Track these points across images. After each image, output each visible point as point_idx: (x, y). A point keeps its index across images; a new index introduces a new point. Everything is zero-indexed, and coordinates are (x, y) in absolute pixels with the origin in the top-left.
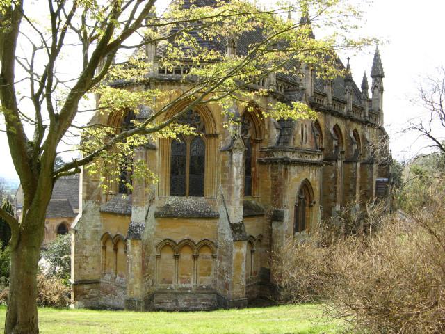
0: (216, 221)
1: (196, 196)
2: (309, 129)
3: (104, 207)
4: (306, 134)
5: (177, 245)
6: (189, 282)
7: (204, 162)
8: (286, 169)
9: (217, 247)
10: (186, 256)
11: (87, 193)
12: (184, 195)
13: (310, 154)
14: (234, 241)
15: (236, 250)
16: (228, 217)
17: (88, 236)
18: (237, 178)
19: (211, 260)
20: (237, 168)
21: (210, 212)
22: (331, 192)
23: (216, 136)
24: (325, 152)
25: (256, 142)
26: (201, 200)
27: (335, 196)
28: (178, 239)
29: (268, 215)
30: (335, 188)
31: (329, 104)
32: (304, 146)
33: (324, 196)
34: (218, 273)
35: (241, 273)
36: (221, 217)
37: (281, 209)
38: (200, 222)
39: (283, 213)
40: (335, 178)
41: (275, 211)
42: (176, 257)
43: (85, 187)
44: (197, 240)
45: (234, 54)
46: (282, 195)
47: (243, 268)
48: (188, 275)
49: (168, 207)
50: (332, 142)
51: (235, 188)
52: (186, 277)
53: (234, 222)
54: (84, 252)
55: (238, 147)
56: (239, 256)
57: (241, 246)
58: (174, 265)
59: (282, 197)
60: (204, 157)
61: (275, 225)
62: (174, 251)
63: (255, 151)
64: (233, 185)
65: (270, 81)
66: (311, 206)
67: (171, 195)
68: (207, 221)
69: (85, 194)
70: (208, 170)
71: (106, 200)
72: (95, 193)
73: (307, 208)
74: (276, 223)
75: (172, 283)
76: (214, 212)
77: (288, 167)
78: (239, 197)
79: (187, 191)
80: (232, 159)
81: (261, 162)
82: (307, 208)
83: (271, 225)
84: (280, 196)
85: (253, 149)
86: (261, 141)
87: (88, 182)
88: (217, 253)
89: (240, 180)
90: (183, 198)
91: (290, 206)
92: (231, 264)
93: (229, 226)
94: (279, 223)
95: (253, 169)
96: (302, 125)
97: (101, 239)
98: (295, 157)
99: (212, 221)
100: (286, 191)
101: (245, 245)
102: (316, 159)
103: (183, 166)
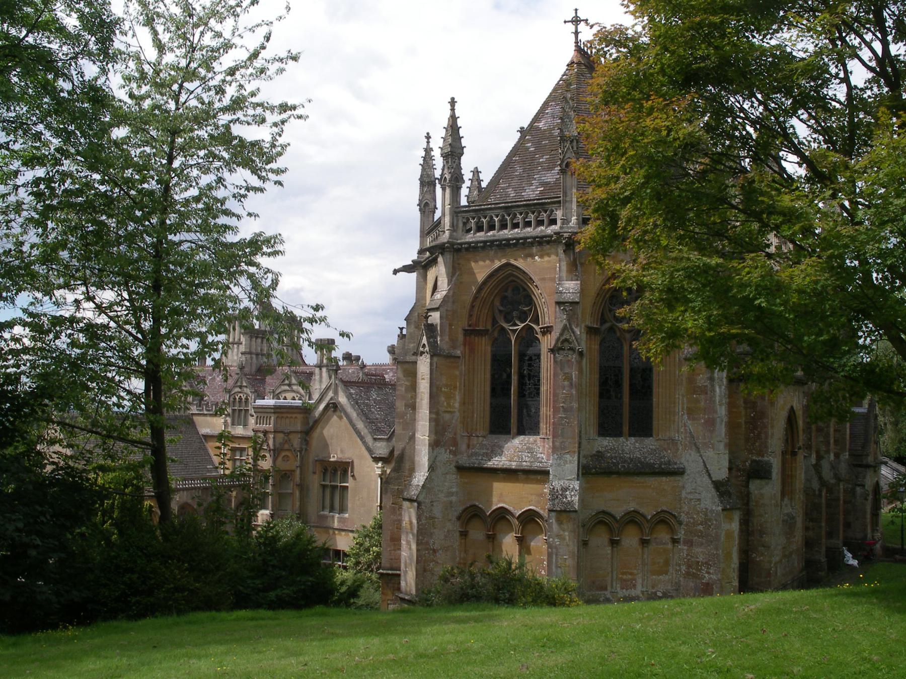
1: (640, 436)
3: (464, 460)
5: (648, 521)
6: (635, 586)
9: (680, 523)
10: (630, 539)
11: (436, 433)
12: (620, 435)
14: (723, 510)
15: (726, 526)
16: (707, 471)
17: (437, 512)
18: (720, 405)
19: (670, 546)
20: (720, 387)
21: (669, 462)
26: (650, 443)
28: (619, 511)
34: (684, 568)
35: (733, 566)
36: (688, 472)
37: (766, 459)
38: (653, 481)
41: (753, 461)
42: (614, 543)
43: (433, 424)
44: (649, 512)
47: (313, 623)
48: (631, 574)
49: (599, 455)
51: (718, 419)
52: (630, 577)
53: (717, 479)
54: (431, 541)
56: (729, 535)
57: (731, 520)
58: (609, 556)
59: (767, 437)
62: (611, 530)
67: (599, 436)
68: (664, 479)
69: (433, 437)
71: (468, 446)
72: (449, 435)
74: (758, 482)
75: (606, 589)
76: (676, 464)
78: (723, 435)
79: (626, 429)
83: (747, 486)
84: (763, 436)
87: (437, 413)
88: (681, 534)
89: (723, 407)
90: (622, 439)
92: (717, 549)
93: (711, 486)
94: (763, 482)
97: (459, 518)
99: (672, 478)
100: (772, 427)
103: (618, 384)
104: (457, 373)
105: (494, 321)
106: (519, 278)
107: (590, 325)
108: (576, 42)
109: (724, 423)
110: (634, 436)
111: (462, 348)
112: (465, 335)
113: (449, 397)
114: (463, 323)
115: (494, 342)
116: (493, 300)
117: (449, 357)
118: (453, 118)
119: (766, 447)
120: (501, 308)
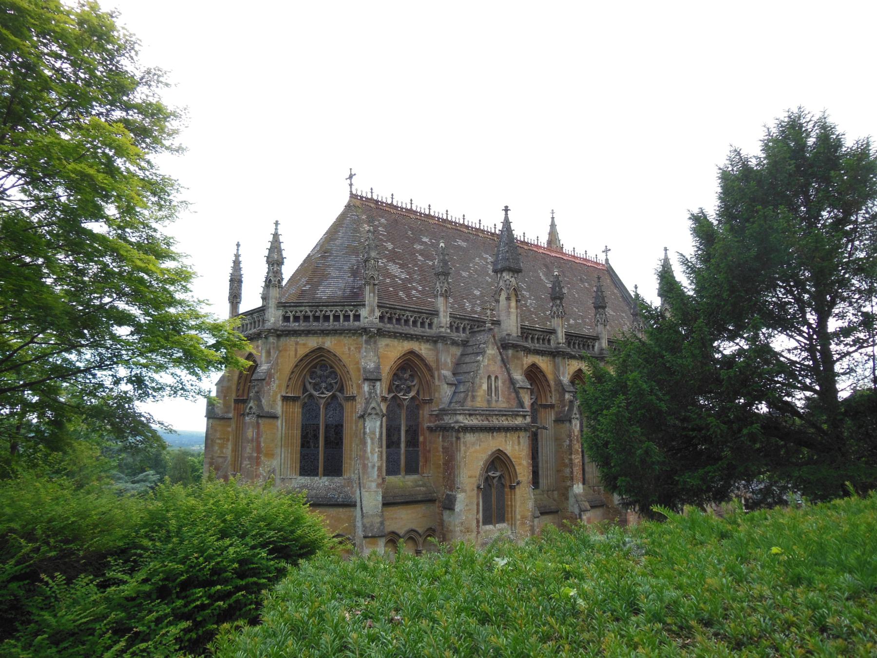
0: (352, 509)
1: (333, 476)
2: (503, 383)
4: (496, 388)
7: (342, 431)
8: (458, 438)
12: (317, 475)
13: (505, 415)
20: (372, 439)
22: (565, 466)
23: (353, 398)
24: (556, 409)
25: (426, 402)
27: (572, 472)
29: (440, 502)
30: (571, 460)
31: (559, 343)
32: (494, 404)
33: (558, 471)
39: (455, 498)
40: (570, 446)
41: (447, 495)
45: (374, 293)
46: (454, 473)
50: (564, 395)
55: (374, 412)
59: (454, 477)
60: (342, 426)
61: (446, 513)
63: (423, 414)
64: (366, 462)
65: (440, 323)
66: (512, 488)
67: (301, 474)
70: (346, 441)
73: (507, 490)
77: (461, 435)
79: (321, 469)
80: (364, 428)
81: (430, 429)
82: (507, 490)
85: (421, 412)
86: (431, 401)
90: (316, 478)
91: (468, 488)
95: (421, 439)
96: (489, 377)
98: (474, 422)
99: (347, 509)
101: (382, 542)
102: (519, 421)
103: (316, 437)
104: (230, 429)
105: (305, 390)
106: (328, 358)
107: (284, 394)
108: (351, 191)
109: (376, 469)
110: (328, 475)
111: (233, 412)
112: (283, 400)
113: (222, 447)
114: (234, 396)
115: (304, 406)
116: (305, 375)
117: (223, 418)
118: (237, 256)
119: (454, 484)
120: (311, 381)
